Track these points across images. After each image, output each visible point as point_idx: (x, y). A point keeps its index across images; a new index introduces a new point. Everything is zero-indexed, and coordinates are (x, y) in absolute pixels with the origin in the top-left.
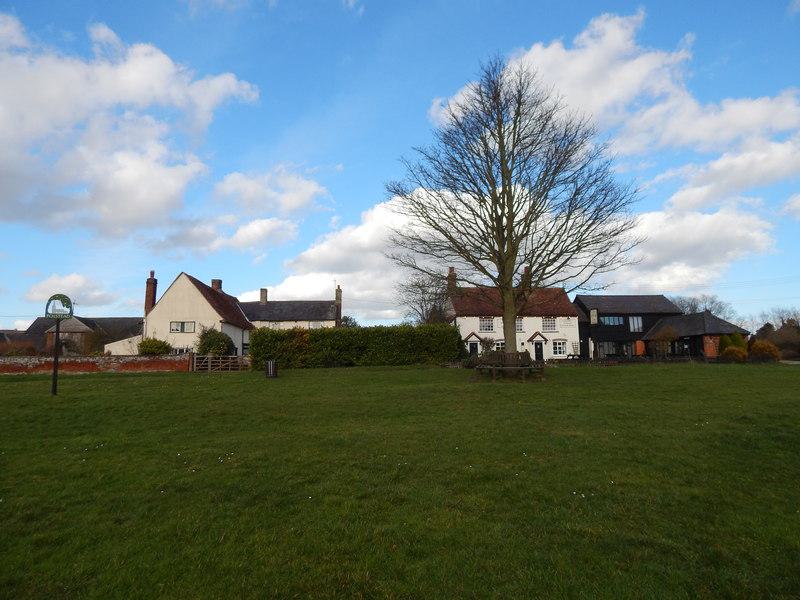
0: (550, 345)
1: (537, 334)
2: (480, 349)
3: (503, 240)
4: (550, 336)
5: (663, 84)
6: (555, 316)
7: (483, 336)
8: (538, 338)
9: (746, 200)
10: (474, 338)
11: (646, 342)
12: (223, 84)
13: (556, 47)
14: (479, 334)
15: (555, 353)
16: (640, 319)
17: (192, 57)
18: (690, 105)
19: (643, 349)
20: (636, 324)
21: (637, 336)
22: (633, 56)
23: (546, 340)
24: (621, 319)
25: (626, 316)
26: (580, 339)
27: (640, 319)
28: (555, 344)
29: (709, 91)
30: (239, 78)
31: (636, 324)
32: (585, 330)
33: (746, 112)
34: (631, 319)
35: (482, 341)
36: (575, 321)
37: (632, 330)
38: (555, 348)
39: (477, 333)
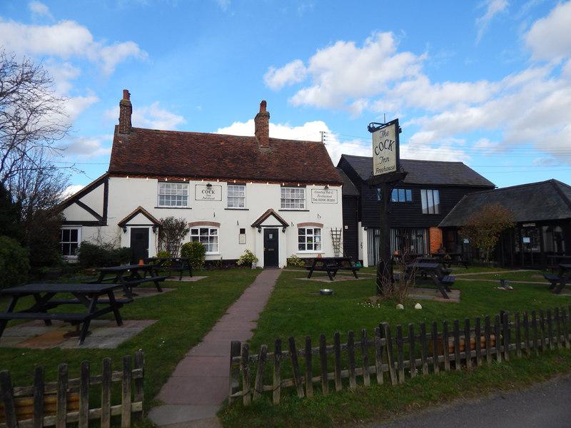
0: (293, 234)
1: (270, 213)
2: (153, 239)
3: (472, 358)
4: (293, 219)
5: (414, 70)
6: (304, 183)
7: (161, 215)
8: (271, 221)
9: (457, 141)
10: (140, 220)
11: (445, 230)
12: (127, 49)
13: (351, 45)
14: (282, 215)
15: (302, 247)
16: (436, 193)
17: (104, 30)
18: (424, 81)
19: (440, 240)
20: (430, 201)
21: (430, 221)
22: (392, 55)
23: (285, 225)
24: (409, 192)
25: (416, 188)
26: (344, 224)
27: (436, 193)
28: (301, 231)
29: (437, 77)
30: (141, 48)
31: (430, 201)
32: (353, 212)
33: (456, 90)
34: (423, 193)
35: (156, 225)
36: (336, 193)
37: (424, 212)
38: (301, 239)
39: (276, 211)
